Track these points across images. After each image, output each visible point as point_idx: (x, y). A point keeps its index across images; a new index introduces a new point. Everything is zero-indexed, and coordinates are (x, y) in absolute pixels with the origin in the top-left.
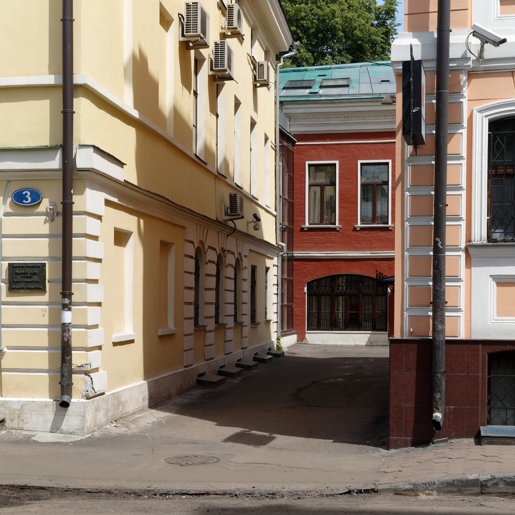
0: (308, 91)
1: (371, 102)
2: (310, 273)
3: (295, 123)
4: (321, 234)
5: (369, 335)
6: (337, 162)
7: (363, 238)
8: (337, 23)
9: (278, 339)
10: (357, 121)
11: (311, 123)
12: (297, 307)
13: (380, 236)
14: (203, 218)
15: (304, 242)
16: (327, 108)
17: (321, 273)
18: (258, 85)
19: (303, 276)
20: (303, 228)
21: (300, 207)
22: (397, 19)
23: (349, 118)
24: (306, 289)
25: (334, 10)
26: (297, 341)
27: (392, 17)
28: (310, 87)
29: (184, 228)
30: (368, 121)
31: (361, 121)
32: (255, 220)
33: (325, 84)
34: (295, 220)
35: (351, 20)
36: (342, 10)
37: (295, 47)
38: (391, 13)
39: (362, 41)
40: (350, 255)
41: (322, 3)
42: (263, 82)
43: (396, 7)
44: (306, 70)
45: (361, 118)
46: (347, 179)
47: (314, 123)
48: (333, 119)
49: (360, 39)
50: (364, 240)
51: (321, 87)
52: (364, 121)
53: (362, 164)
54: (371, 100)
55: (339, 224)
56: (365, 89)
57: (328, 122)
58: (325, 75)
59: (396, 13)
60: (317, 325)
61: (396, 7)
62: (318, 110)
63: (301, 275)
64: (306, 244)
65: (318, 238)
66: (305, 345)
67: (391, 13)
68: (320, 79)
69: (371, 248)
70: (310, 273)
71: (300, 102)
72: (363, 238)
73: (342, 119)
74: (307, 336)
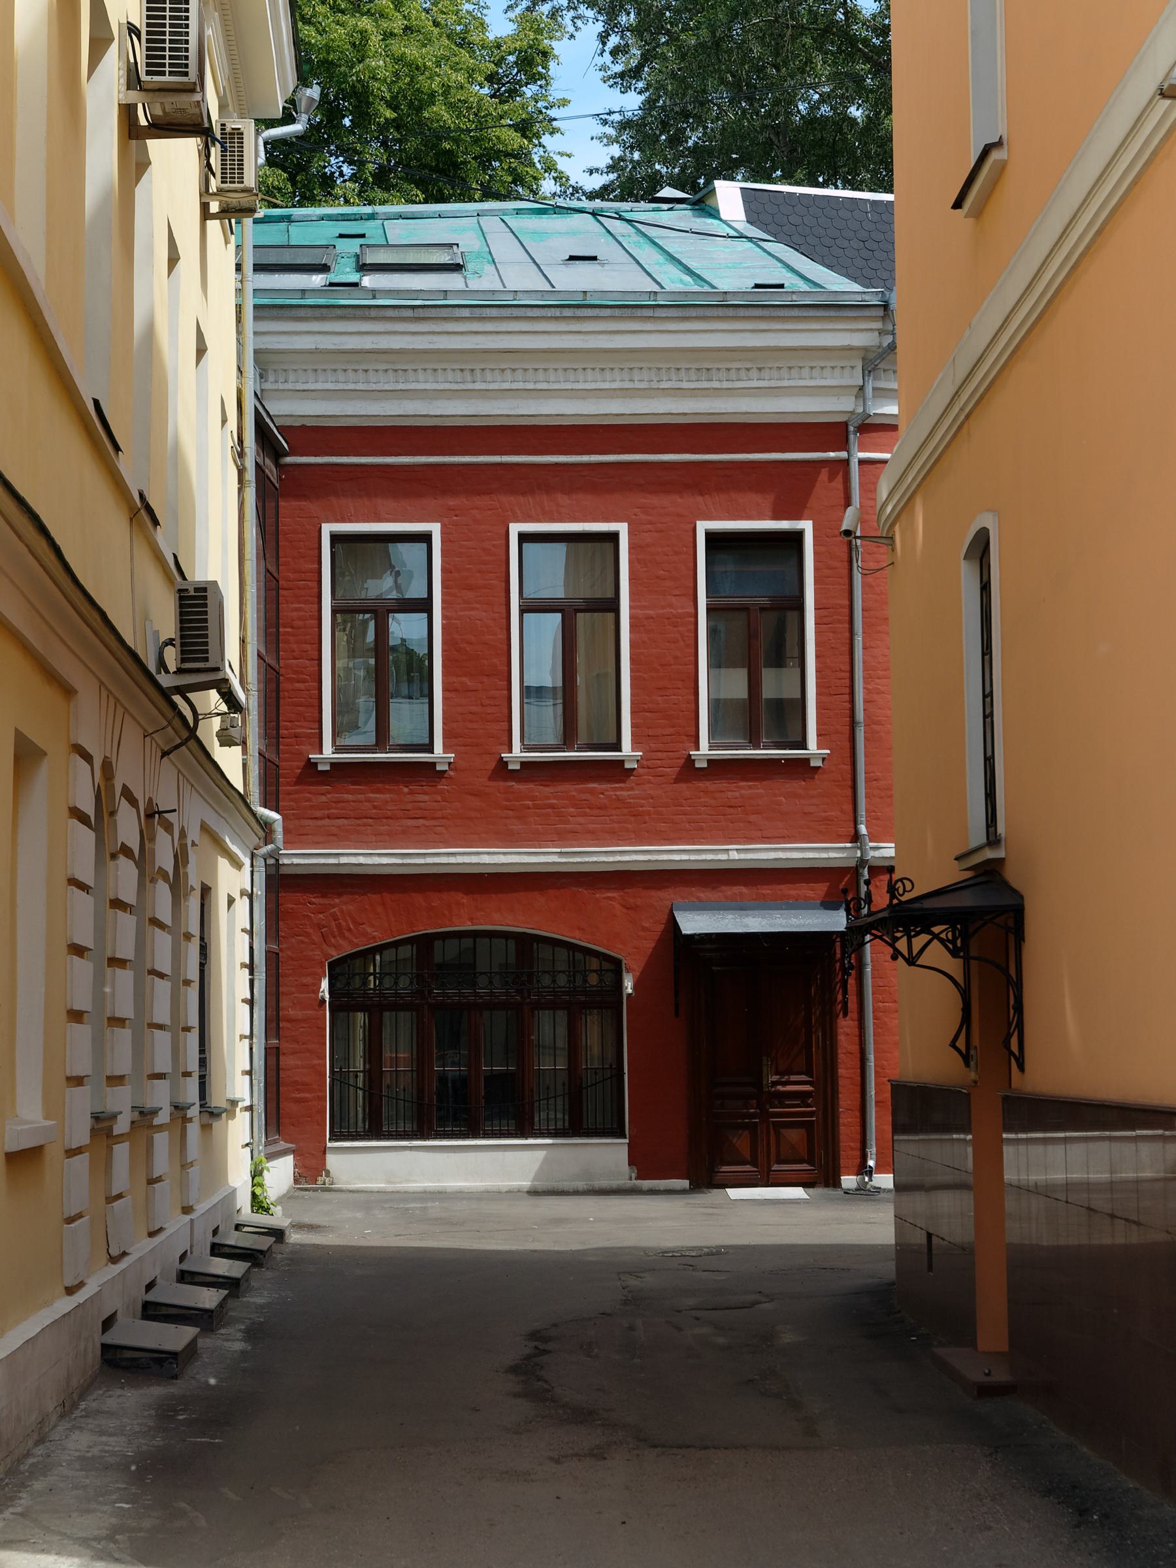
0: (317, 280)
1: (556, 318)
2: (339, 926)
3: (281, 387)
4: (388, 785)
5: (541, 1154)
6: (435, 529)
7: (533, 799)
8: (374, 78)
9: (257, 1173)
10: (506, 386)
11: (341, 386)
12: (294, 1053)
13: (592, 791)
14: (128, 661)
15: (318, 814)
16: (398, 338)
17: (378, 926)
18: (214, 207)
19: (316, 938)
20: (316, 764)
21: (301, 686)
22: (555, 85)
23: (478, 372)
24: (325, 984)
25: (363, 33)
26: (296, 1181)
27: (542, 78)
28: (324, 268)
29: (69, 692)
30: (544, 386)
31: (520, 385)
32: (224, 708)
33: (370, 258)
34: (283, 732)
35: (418, 68)
36: (388, 35)
37: (303, 106)
38: (539, 59)
39: (456, 141)
40: (486, 859)
41: (320, 9)
42: (235, 199)
43: (554, 44)
44: (288, 219)
45: (519, 375)
46: (470, 588)
47: (351, 386)
48: (421, 375)
49: (444, 133)
50: (536, 807)
51: (364, 268)
52: (531, 386)
53: (524, 538)
54: (557, 312)
55: (446, 748)
56: (521, 279)
57: (401, 386)
58: (363, 236)
59: (552, 64)
60: (377, 1116)
61: (554, 44)
62: (368, 343)
63: (308, 935)
64: (326, 822)
65: (369, 800)
66: (327, 1195)
67: (539, 59)
68: (353, 246)
69: (562, 837)
70: (339, 926)
71: (302, 313)
72: (533, 799)
73: (450, 376)
74: (332, 1160)
